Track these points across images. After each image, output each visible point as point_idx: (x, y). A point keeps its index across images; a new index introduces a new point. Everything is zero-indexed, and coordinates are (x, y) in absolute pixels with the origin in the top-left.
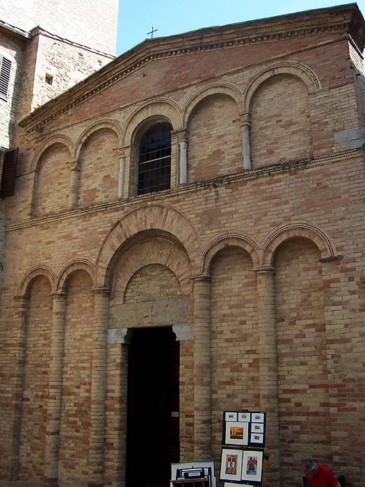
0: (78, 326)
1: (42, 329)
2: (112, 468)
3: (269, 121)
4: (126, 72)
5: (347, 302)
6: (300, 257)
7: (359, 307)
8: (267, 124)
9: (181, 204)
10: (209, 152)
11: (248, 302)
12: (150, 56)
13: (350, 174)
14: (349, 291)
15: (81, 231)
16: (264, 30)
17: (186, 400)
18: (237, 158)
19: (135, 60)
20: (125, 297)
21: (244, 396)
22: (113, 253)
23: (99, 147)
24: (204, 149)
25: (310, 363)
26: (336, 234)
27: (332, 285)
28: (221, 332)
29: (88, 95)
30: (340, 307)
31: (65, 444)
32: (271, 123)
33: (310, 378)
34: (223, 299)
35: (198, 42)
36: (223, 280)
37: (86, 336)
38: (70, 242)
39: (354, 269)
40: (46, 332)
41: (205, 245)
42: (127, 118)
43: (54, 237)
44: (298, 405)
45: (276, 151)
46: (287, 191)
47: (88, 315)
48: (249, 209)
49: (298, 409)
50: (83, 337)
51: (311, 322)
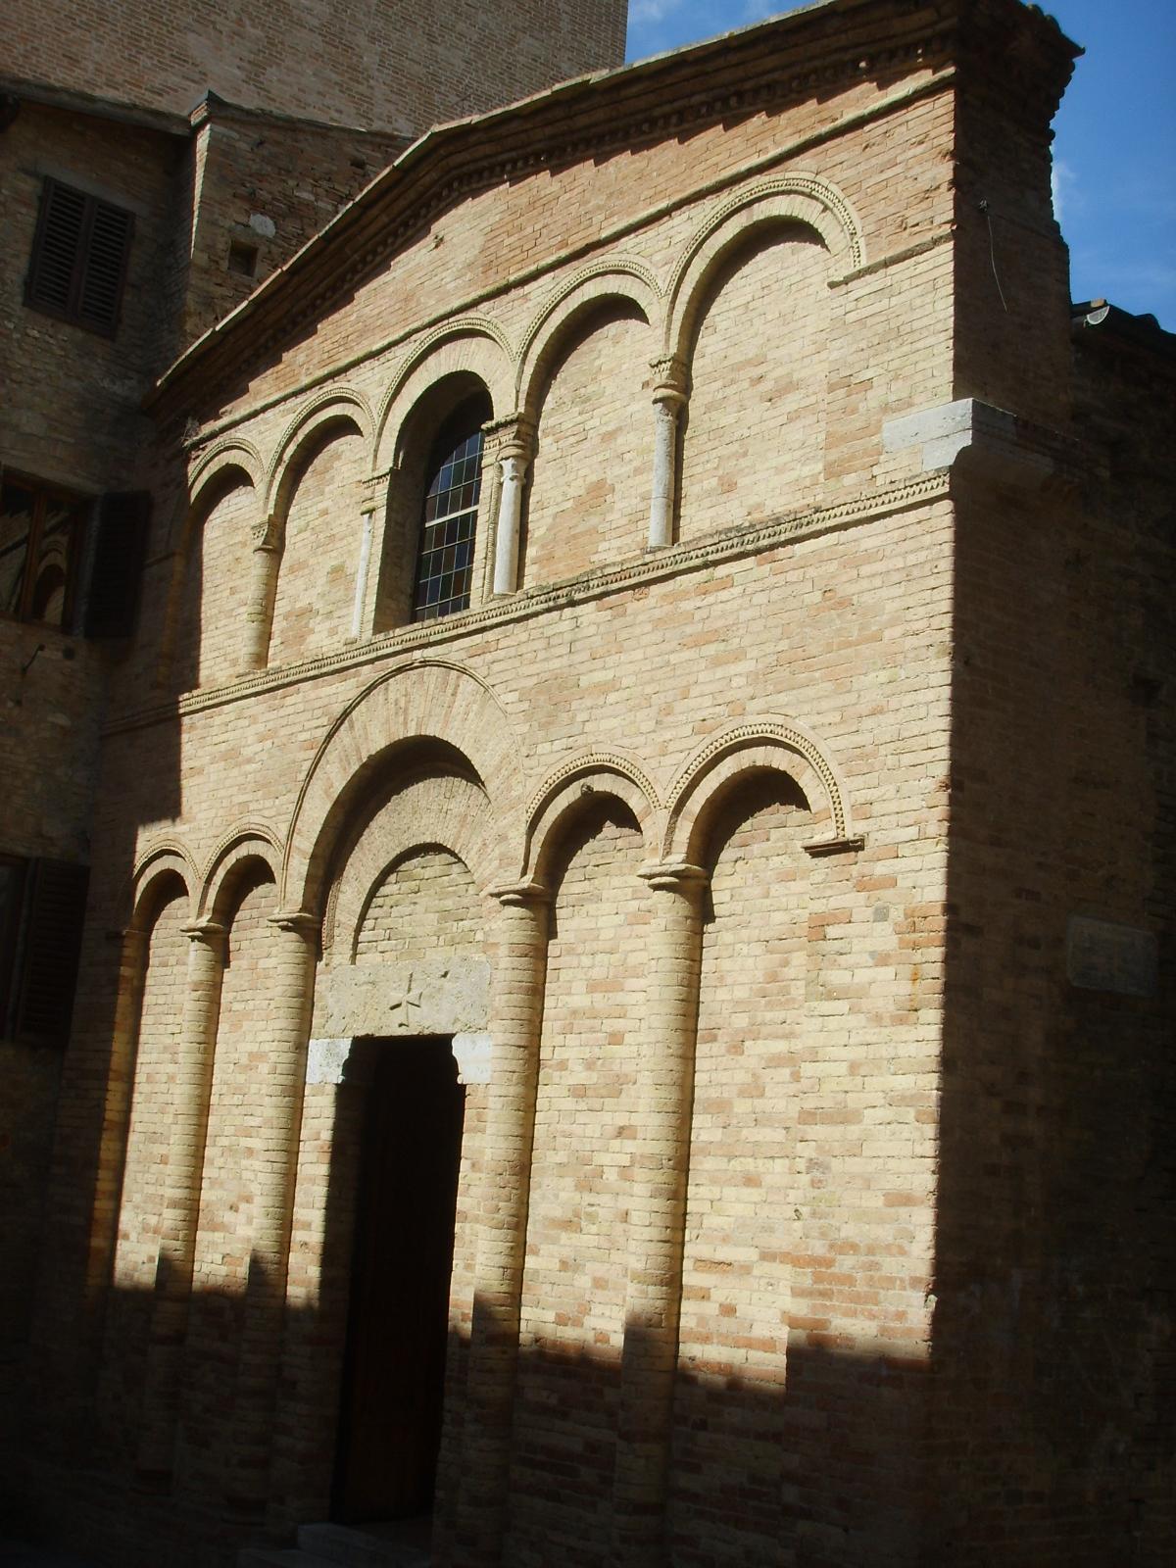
0: (246, 1025)
4: (395, 234)
6: (775, 834)
9: (489, 657)
13: (912, 559)
14: (872, 954)
19: (412, 195)
20: (356, 943)
22: (328, 806)
25: (768, 1180)
27: (831, 931)
30: (843, 1006)
42: (387, 382)
44: (729, 1310)
46: (745, 615)
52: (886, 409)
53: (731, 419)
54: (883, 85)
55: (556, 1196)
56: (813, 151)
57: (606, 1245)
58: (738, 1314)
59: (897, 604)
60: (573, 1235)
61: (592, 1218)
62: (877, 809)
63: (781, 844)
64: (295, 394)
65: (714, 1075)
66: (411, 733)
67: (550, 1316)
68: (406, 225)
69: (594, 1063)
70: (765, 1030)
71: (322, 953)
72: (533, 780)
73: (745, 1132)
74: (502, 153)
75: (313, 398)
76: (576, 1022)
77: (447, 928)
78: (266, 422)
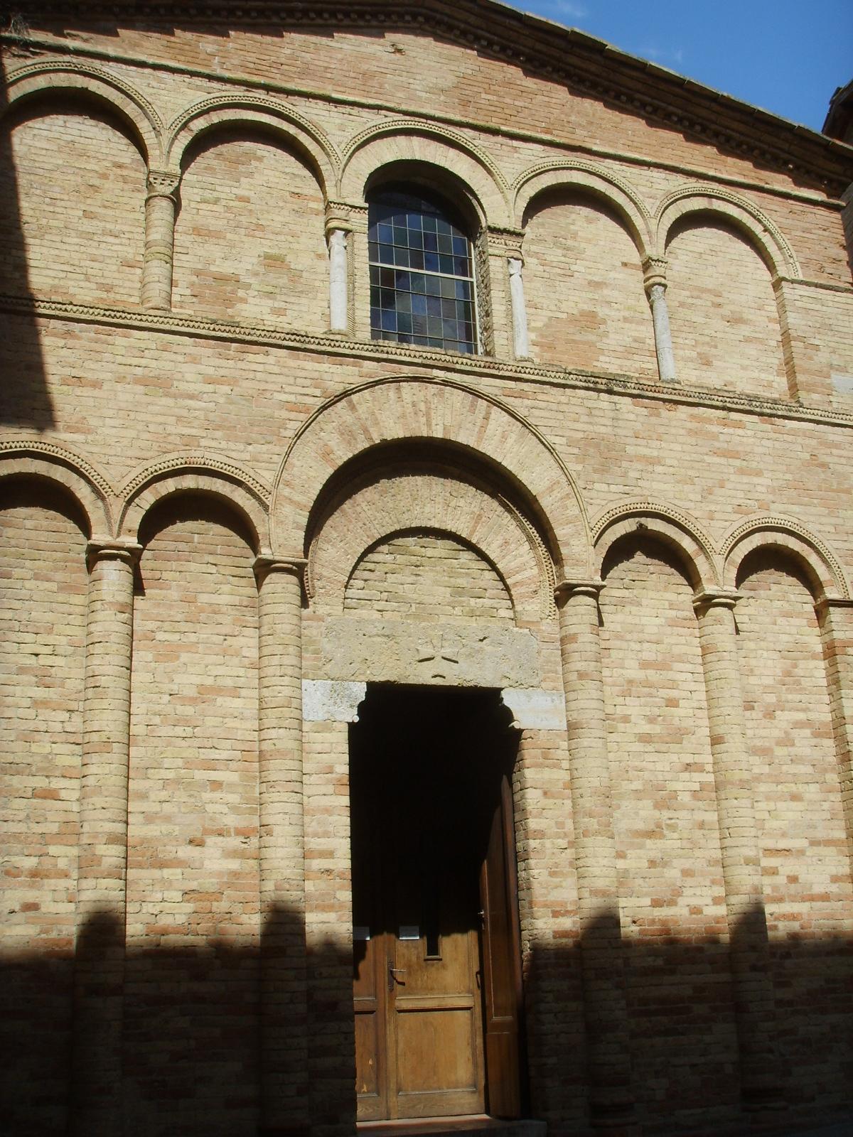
0: (184, 657)
3: (698, 297)
6: (774, 587)
8: (694, 301)
9: (527, 402)
11: (681, 659)
12: (420, 14)
17: (552, 874)
21: (687, 864)
23: (242, 168)
25: (807, 796)
28: (626, 719)
32: (698, 302)
33: (810, 827)
34: (624, 645)
37: (219, 691)
38: (170, 402)
40: (43, 660)
41: (598, 516)
44: (793, 879)
45: (715, 363)
47: (224, 630)
49: (793, 888)
50: (205, 694)
51: (801, 716)
54: (798, 183)
55: (637, 814)
56: (756, 193)
57: (689, 846)
58: (800, 881)
60: (658, 841)
61: (673, 828)
63: (780, 594)
65: (757, 731)
66: (438, 434)
67: (647, 901)
69: (655, 719)
71: (308, 601)
74: (482, 29)
75: (238, 93)
76: (634, 689)
77: (464, 602)
78: (160, 81)
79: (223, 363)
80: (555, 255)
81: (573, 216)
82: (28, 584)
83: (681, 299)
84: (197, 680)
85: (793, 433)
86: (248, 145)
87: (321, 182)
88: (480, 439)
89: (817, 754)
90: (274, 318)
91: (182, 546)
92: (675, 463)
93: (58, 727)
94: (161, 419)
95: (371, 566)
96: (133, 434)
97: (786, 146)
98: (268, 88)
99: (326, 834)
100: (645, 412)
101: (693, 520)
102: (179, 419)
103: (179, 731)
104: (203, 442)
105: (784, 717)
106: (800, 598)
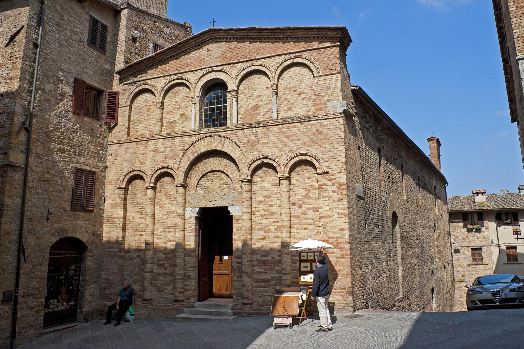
0: (165, 206)
1: (139, 208)
2: (190, 290)
3: (289, 90)
5: (331, 197)
6: (305, 171)
7: (337, 199)
8: (288, 92)
9: (234, 136)
10: (251, 105)
11: (275, 194)
13: (335, 127)
14: (332, 191)
15: (166, 148)
16: (289, 34)
18: (268, 110)
19: (201, 40)
23: (177, 94)
24: (248, 103)
26: (327, 159)
27: (323, 187)
28: (258, 211)
29: (168, 59)
30: (327, 199)
31: (158, 278)
34: (259, 192)
35: (246, 34)
36: (260, 181)
37: (170, 212)
38: (159, 154)
39: (335, 179)
41: (249, 161)
43: (146, 151)
46: (298, 133)
47: (172, 200)
48: (276, 142)
50: (168, 213)
51: (310, 206)
52: (328, 100)
53: (289, 97)
59: (332, 134)
61: (269, 237)
62: (331, 167)
64: (167, 76)
66: (213, 148)
67: (260, 256)
68: (199, 45)
70: (306, 203)
72: (249, 160)
73: (303, 221)
75: (173, 77)
78: (158, 80)
79: (169, 143)
80: (248, 92)
81: (254, 78)
82: (139, 195)
83: (283, 93)
84: (166, 211)
85: (311, 125)
86: (178, 88)
87: (269, 78)
88: (222, 147)
89: (314, 216)
90: (182, 129)
91: (164, 183)
92: (272, 142)
93: (143, 222)
94: (157, 158)
95: (202, 181)
96: (152, 162)
97: (316, 33)
98: (179, 74)
99: (189, 241)
100: (265, 130)
101: (276, 157)
102: (160, 157)
103: (163, 221)
104: (164, 162)
105: (304, 207)
106: (313, 173)
